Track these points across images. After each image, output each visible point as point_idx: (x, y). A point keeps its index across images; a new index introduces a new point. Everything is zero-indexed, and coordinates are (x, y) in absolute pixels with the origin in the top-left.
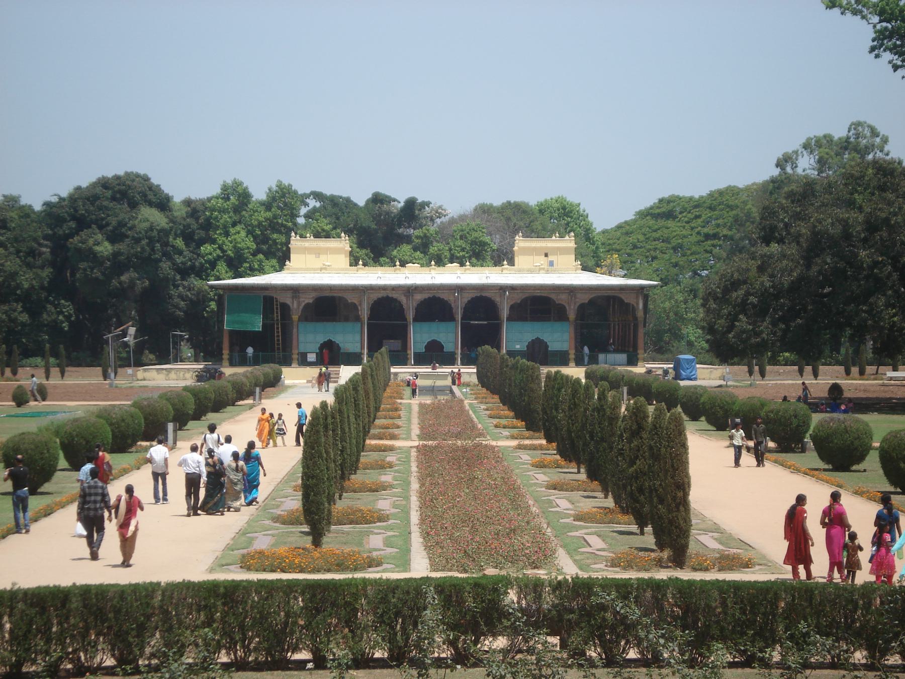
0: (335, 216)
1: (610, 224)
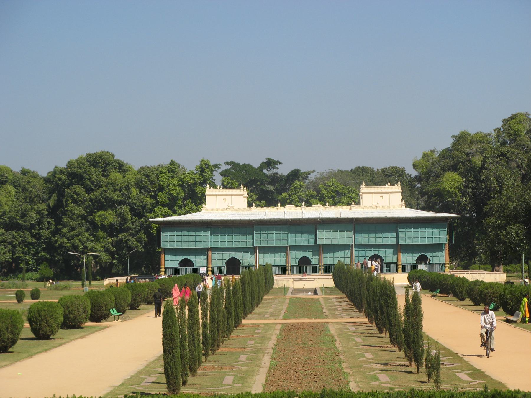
0: (238, 175)
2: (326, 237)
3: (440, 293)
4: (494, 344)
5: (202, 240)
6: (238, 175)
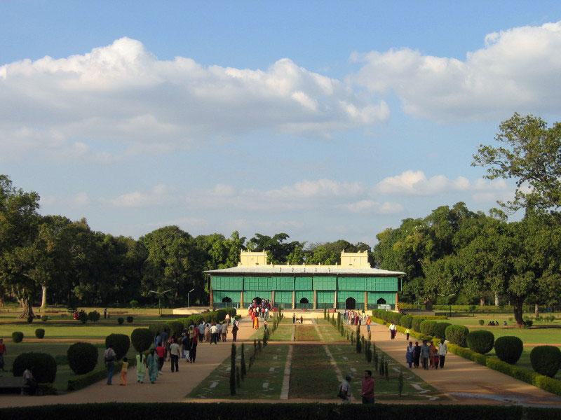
0: (262, 243)
1: (359, 254)
2: (319, 284)
3: (58, 304)
4: (390, 334)
5: (236, 283)
6: (262, 243)
